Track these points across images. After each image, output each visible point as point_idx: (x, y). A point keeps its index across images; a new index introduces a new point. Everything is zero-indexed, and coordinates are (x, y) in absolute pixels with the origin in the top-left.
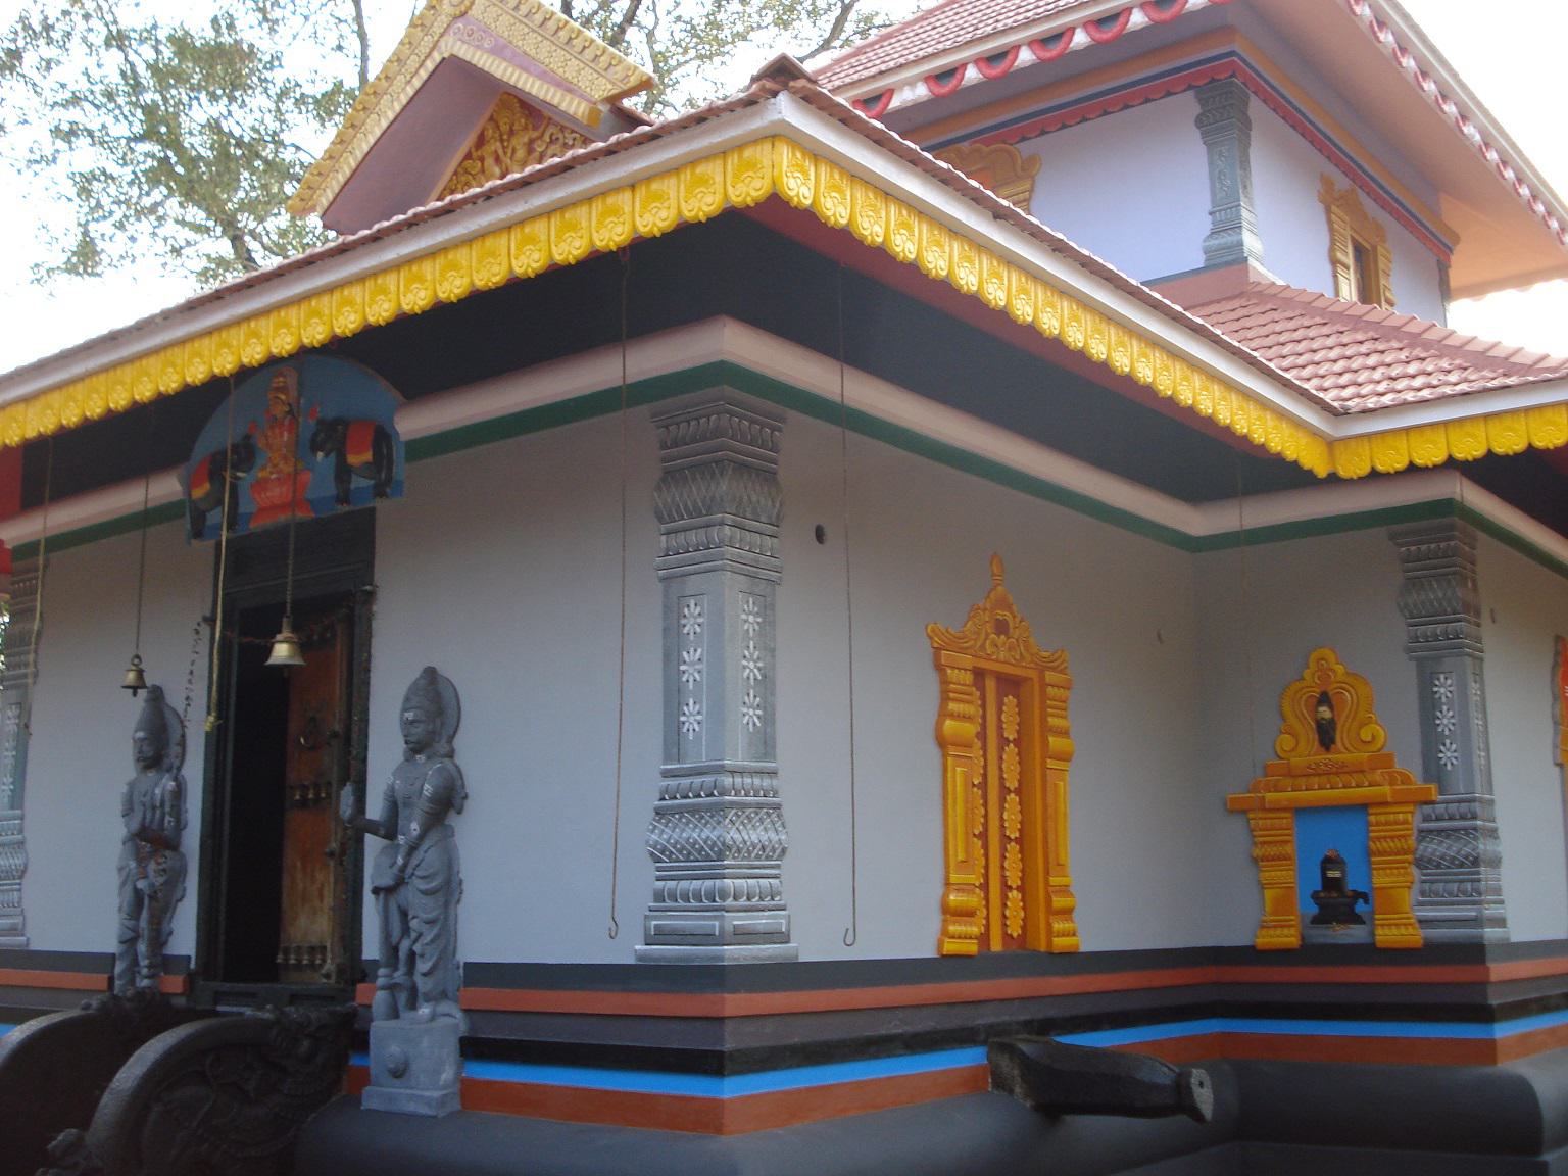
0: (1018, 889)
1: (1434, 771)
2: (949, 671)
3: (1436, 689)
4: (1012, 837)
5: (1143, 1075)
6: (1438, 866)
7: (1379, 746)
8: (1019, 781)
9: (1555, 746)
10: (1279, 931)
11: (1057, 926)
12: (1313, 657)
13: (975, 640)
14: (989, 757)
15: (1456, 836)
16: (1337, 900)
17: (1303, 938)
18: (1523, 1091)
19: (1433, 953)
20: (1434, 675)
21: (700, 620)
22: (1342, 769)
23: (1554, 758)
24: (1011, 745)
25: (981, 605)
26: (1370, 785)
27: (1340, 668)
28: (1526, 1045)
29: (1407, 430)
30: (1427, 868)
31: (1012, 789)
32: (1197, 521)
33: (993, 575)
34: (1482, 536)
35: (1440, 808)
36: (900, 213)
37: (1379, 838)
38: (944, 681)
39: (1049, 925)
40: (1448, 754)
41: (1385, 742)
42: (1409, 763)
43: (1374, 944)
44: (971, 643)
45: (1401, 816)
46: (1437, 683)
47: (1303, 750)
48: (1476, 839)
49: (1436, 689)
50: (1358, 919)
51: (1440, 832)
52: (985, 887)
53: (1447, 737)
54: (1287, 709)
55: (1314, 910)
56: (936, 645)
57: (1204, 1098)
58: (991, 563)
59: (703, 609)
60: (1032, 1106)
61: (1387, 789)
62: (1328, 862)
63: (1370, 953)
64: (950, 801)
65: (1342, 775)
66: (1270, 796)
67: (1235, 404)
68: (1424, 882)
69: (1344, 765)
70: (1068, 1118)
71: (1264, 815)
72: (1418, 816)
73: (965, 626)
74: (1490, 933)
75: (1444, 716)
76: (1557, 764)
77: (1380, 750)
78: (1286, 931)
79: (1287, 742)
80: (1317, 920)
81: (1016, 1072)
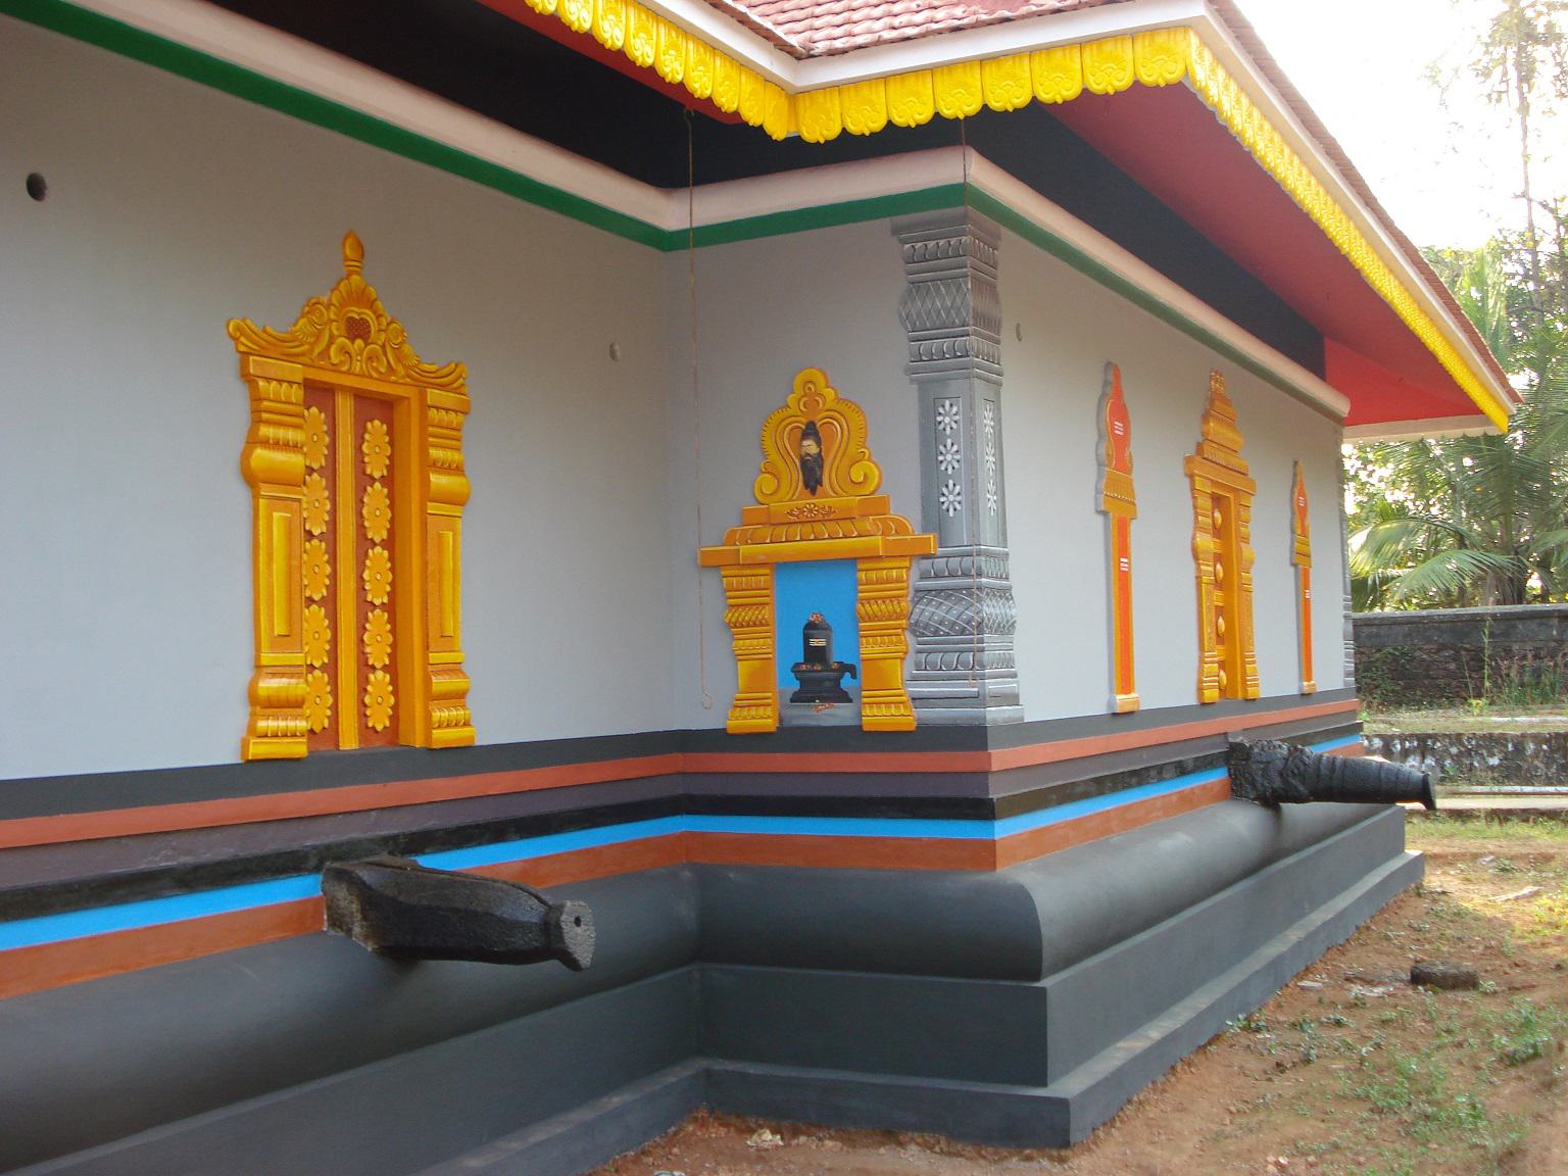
0: (385, 668)
1: (935, 519)
2: (261, 383)
3: (939, 419)
4: (377, 602)
5: (505, 911)
6: (936, 633)
7: (872, 489)
8: (388, 530)
9: (1098, 491)
10: (753, 712)
11: (438, 715)
12: (800, 378)
13: (313, 345)
14: (340, 499)
15: (957, 592)
16: (821, 675)
17: (781, 720)
18: (1021, 899)
19: (928, 737)
20: (938, 401)
21: (958, 457)
22: (828, 516)
23: (1096, 504)
24: (377, 485)
25: (325, 300)
26: (860, 536)
27: (830, 393)
28: (1038, 843)
29: (885, 78)
30: (923, 635)
31: (377, 540)
32: (669, 211)
33: (346, 259)
34: (1005, 232)
35: (940, 563)
36: (640, 17)
37: (868, 600)
38: (256, 398)
39: (428, 715)
40: (951, 498)
41: (878, 486)
42: (906, 508)
43: (861, 727)
44: (306, 347)
45: (894, 573)
46: (941, 410)
47: (788, 494)
48: (980, 600)
49: (939, 419)
50: (844, 697)
51: (939, 591)
52: (332, 668)
53: (950, 477)
54: (769, 445)
55: (796, 686)
56: (242, 349)
57: (581, 941)
58: (344, 245)
59: (959, 446)
60: (373, 949)
61: (878, 540)
62: (811, 628)
63: (855, 737)
64: (262, 558)
65: (827, 523)
66: (744, 549)
67: (692, 57)
68: (919, 652)
69: (830, 511)
70: (432, 963)
71: (736, 572)
72: (915, 573)
73: (295, 325)
74: (994, 714)
75: (948, 452)
76: (1099, 512)
77: (872, 494)
78: (761, 711)
79: (768, 483)
80: (797, 698)
81: (355, 907)
